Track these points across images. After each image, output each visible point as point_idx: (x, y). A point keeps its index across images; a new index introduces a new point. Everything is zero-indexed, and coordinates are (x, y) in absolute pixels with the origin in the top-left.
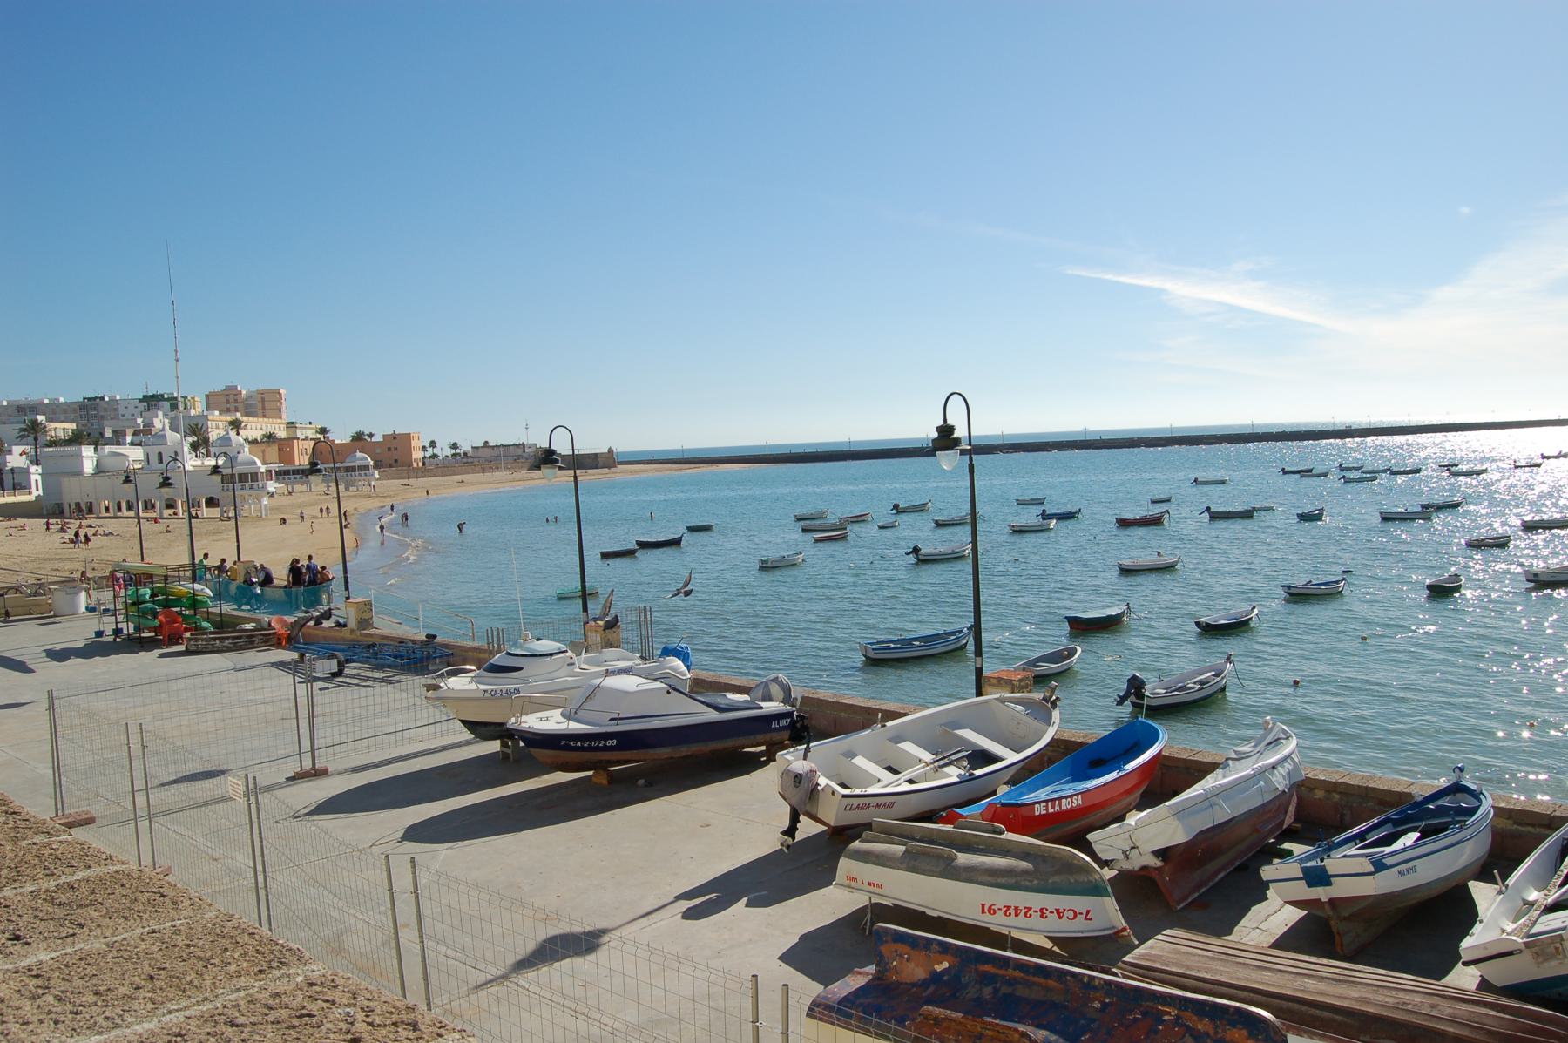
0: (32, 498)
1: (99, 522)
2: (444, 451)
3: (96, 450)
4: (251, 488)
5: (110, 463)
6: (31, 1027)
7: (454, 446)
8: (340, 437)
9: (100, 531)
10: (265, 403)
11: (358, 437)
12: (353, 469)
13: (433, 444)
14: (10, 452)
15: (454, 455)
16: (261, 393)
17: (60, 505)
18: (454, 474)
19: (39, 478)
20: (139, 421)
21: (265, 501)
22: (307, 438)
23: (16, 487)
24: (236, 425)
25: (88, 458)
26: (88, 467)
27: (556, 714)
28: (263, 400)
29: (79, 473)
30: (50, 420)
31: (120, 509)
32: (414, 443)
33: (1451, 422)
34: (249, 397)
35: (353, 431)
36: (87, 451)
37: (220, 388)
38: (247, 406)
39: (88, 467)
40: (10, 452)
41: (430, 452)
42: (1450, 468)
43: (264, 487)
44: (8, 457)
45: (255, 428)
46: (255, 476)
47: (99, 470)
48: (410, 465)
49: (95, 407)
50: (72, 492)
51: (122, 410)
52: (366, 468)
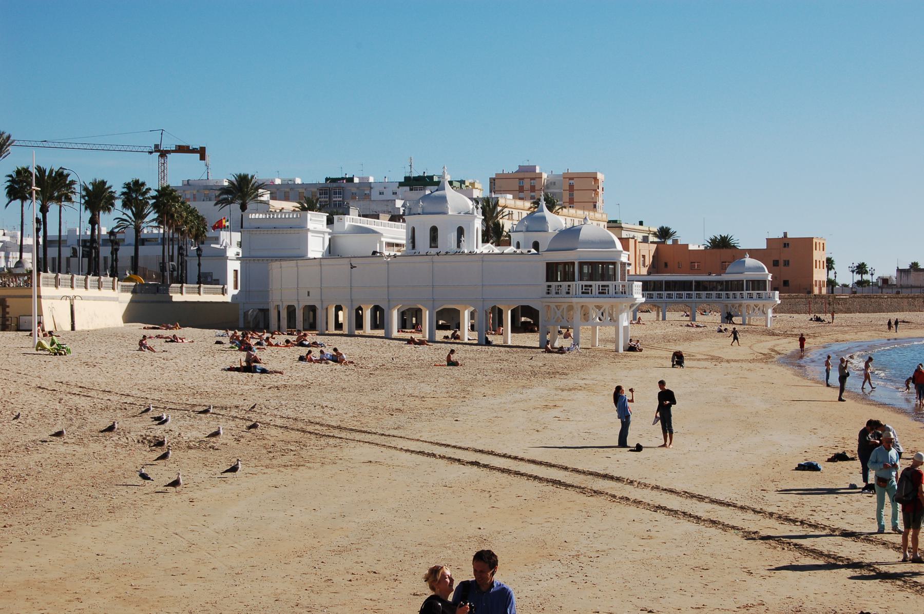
0: (228, 298)
1: (319, 339)
2: (845, 277)
3: (330, 222)
4: (603, 292)
5: (353, 245)
6: (378, 411)
7: (861, 269)
9: (316, 353)
10: (578, 190)
12: (737, 286)
15: (860, 283)
16: (570, 177)
17: (265, 312)
20: (399, 203)
23: (204, 279)
26: (316, 247)
27: (174, 300)
28: (571, 188)
29: (301, 256)
30: (273, 197)
31: (360, 325)
34: (551, 184)
36: (316, 221)
39: (316, 247)
47: (332, 250)
48: (810, 291)
49: (341, 192)
50: (286, 287)
51: (375, 195)
52: (759, 285)
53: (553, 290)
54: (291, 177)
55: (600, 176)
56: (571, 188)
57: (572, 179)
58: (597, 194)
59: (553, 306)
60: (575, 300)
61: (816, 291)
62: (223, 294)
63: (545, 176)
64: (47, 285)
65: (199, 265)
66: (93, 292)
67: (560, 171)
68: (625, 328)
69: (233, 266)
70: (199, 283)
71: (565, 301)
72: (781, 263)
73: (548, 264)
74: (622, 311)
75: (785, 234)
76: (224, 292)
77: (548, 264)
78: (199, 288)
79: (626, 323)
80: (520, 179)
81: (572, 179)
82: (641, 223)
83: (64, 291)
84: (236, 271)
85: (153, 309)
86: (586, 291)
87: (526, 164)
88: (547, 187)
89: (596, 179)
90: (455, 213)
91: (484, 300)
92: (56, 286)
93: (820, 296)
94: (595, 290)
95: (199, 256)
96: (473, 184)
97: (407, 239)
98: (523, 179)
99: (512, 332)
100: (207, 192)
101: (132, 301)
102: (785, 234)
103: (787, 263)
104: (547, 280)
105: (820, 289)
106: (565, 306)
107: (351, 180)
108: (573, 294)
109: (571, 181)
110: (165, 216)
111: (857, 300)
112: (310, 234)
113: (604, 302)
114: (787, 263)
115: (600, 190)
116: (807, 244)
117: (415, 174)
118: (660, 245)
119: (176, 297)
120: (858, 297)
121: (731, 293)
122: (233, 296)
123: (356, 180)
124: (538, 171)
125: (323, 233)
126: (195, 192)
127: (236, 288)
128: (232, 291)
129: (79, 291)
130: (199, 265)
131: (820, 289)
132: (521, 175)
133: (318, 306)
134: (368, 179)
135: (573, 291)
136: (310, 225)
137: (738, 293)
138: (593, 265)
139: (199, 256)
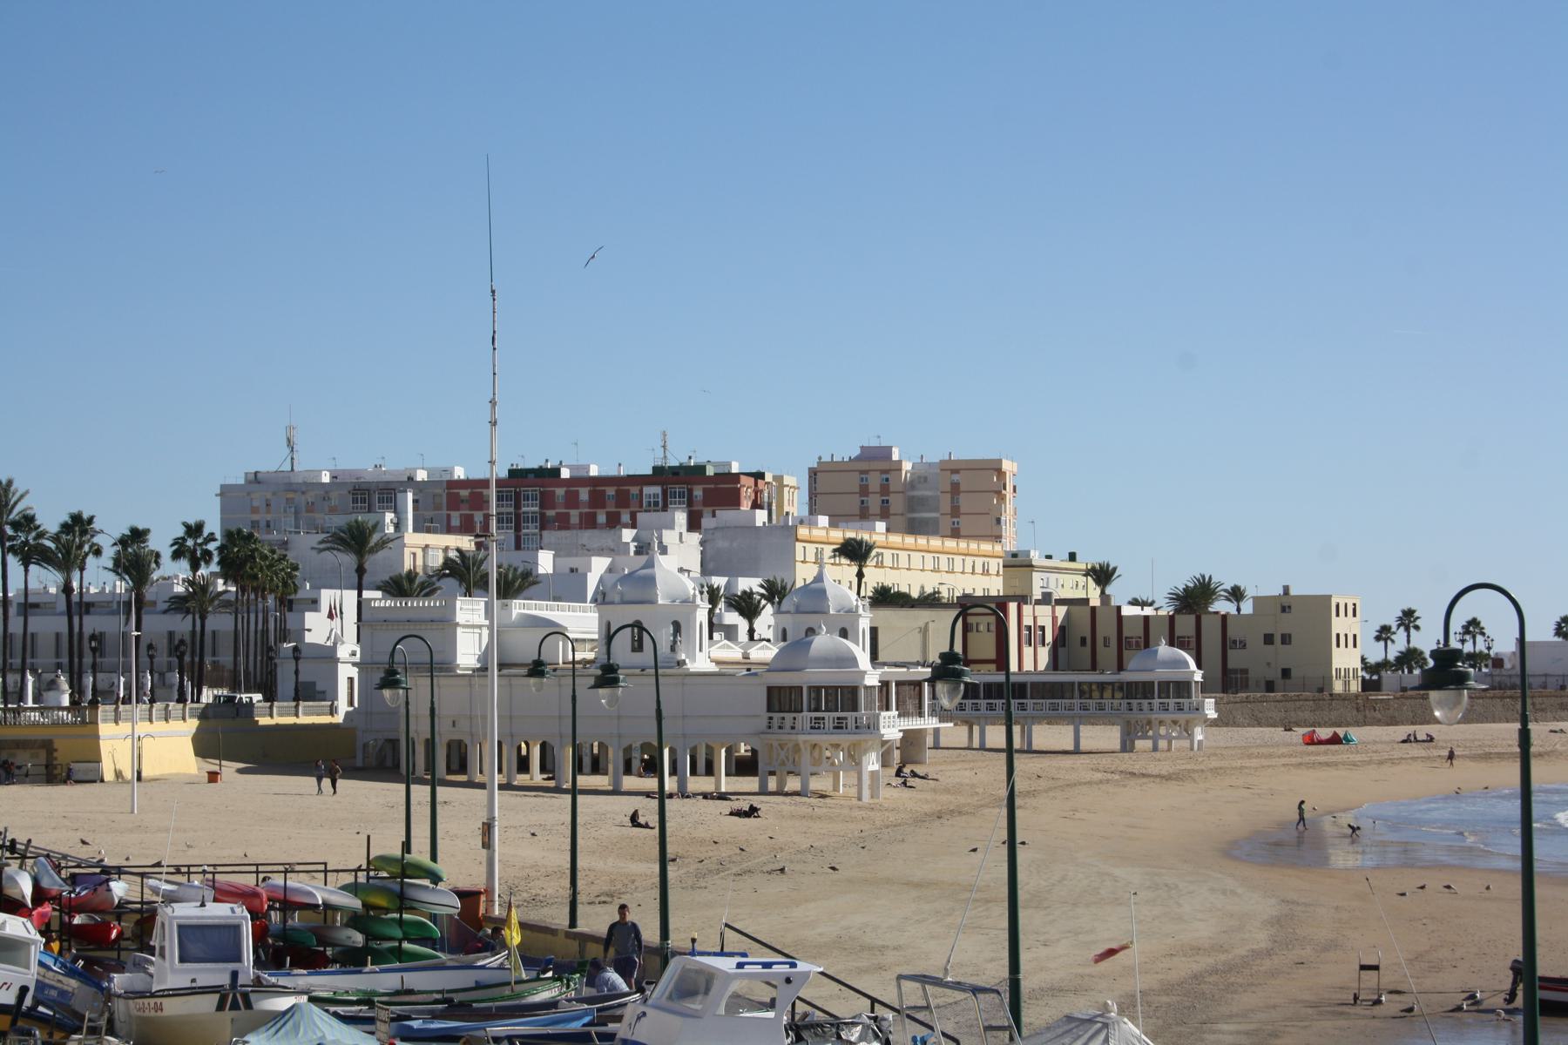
0: (339, 718)
4: (840, 726)
8: (1145, 589)
10: (957, 498)
11: (1195, 598)
12: (1143, 690)
13: (1408, 619)
14: (314, 604)
16: (952, 468)
18: (1393, 722)
19: (354, 672)
21: (1199, 734)
22: (1046, 599)
23: (305, 692)
24: (855, 552)
25: (472, 629)
28: (955, 489)
29: (439, 665)
32: (1339, 625)
33: (1007, 944)
34: (919, 479)
35: (1182, 580)
37: (846, 450)
38: (913, 504)
39: (467, 652)
40: (314, 604)
41: (1399, 644)
42: (1079, 1037)
43: (873, 726)
44: (311, 619)
45: (910, 563)
46: (846, 697)
48: (1323, 686)
52: (1182, 688)
53: (775, 723)
54: (441, 464)
55: (1007, 466)
56: (955, 489)
57: (955, 471)
58: (1002, 498)
59: (775, 744)
60: (801, 738)
61: (1338, 687)
62: (332, 714)
63: (907, 466)
64: (105, 721)
65: (297, 672)
66: (159, 726)
67: (935, 456)
68: (873, 774)
69: (346, 672)
70: (297, 699)
71: (789, 738)
72: (1278, 639)
73: (770, 689)
74: (866, 751)
75: (1286, 589)
76: (333, 711)
77: (770, 689)
78: (297, 707)
79: (876, 767)
80: (862, 472)
81: (955, 471)
82: (1072, 557)
83: (125, 727)
84: (351, 680)
85: (227, 738)
86: (817, 725)
87: (874, 443)
88: (912, 485)
89: (1000, 473)
90: (667, 602)
91: (684, 736)
92: (116, 722)
93: (1345, 698)
94: (829, 724)
95: (297, 659)
96: (779, 479)
97: (600, 633)
98: (866, 472)
99: (727, 775)
100: (290, 495)
101: (198, 729)
102: (1286, 589)
103: (1286, 639)
104: (769, 710)
105: (1346, 684)
106: (790, 745)
107: (556, 472)
108: (801, 730)
109: (956, 477)
110: (231, 568)
111: (1408, 702)
112: (459, 630)
113: (844, 739)
114: (1286, 639)
115: (1009, 492)
116: (1320, 607)
117: (673, 462)
118: (1075, 609)
119: (264, 721)
120: (1411, 697)
121: (1134, 702)
122: (347, 714)
123: (565, 474)
124: (895, 457)
125: (480, 627)
126: (269, 496)
127: (351, 703)
128: (343, 707)
129: (143, 728)
130: (297, 672)
131: (1346, 684)
132: (864, 466)
133: (467, 741)
134: (587, 468)
135: (798, 725)
136: (461, 617)
137: (1145, 702)
138: (832, 690)
139: (297, 659)
